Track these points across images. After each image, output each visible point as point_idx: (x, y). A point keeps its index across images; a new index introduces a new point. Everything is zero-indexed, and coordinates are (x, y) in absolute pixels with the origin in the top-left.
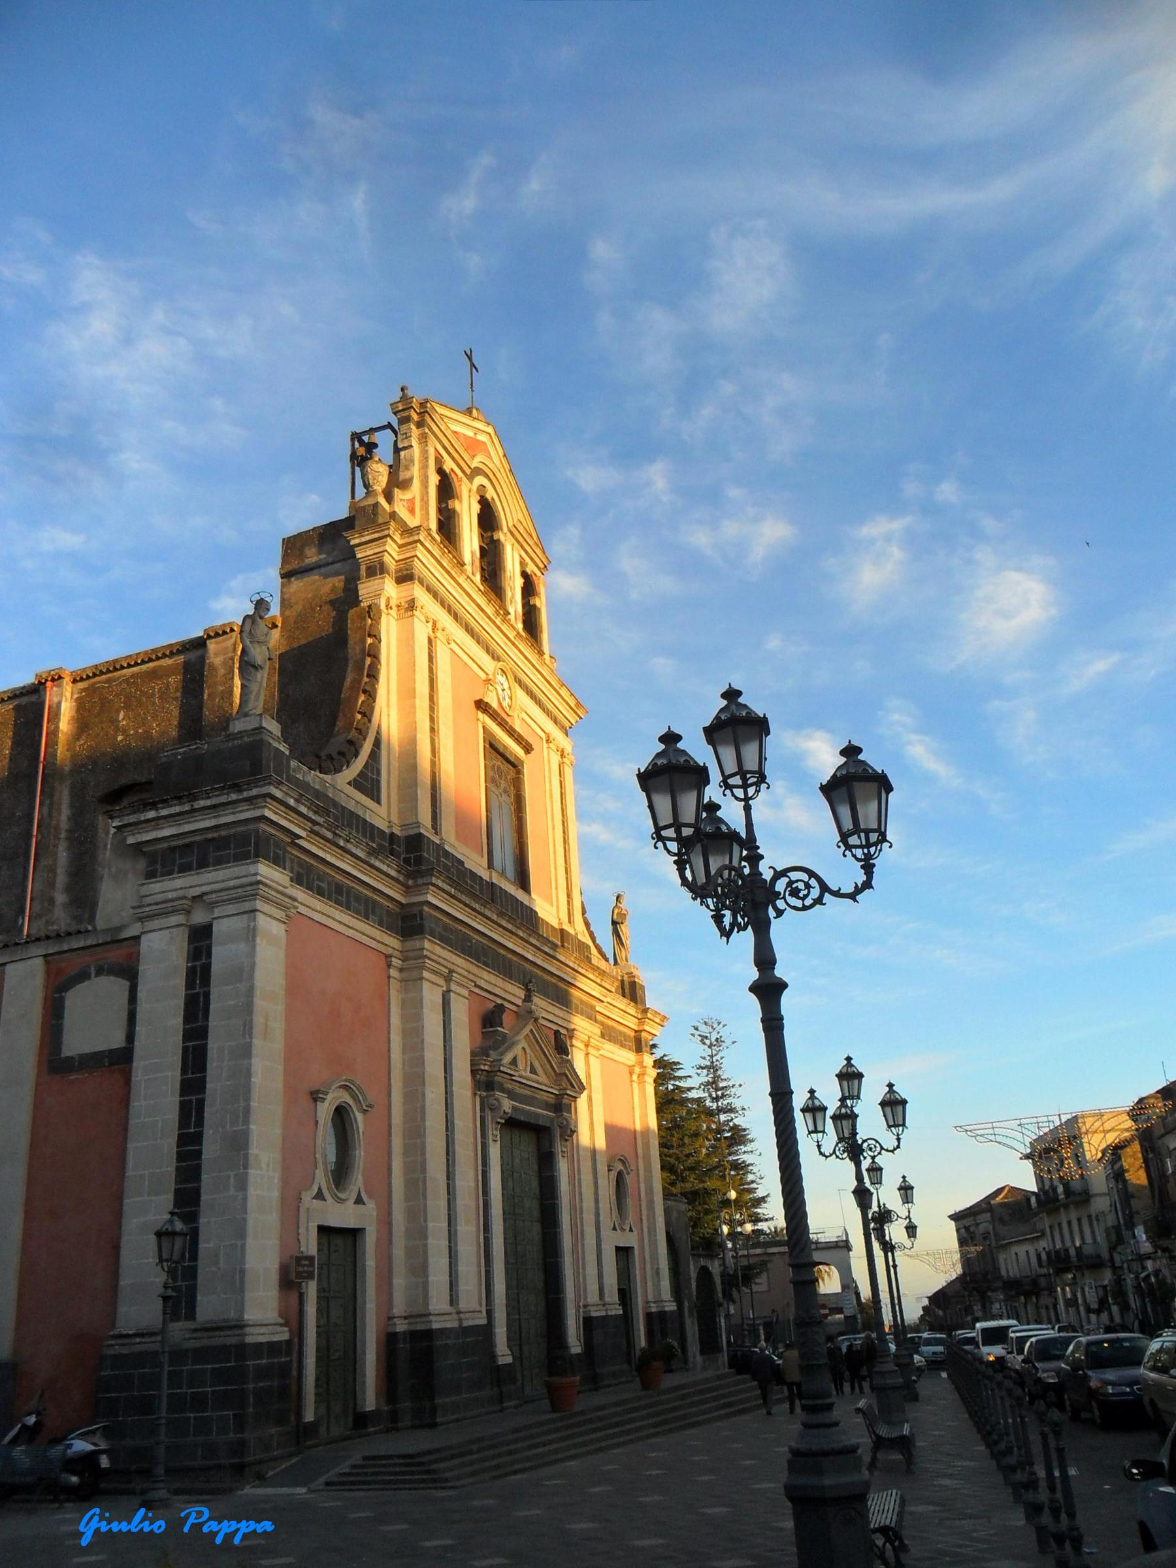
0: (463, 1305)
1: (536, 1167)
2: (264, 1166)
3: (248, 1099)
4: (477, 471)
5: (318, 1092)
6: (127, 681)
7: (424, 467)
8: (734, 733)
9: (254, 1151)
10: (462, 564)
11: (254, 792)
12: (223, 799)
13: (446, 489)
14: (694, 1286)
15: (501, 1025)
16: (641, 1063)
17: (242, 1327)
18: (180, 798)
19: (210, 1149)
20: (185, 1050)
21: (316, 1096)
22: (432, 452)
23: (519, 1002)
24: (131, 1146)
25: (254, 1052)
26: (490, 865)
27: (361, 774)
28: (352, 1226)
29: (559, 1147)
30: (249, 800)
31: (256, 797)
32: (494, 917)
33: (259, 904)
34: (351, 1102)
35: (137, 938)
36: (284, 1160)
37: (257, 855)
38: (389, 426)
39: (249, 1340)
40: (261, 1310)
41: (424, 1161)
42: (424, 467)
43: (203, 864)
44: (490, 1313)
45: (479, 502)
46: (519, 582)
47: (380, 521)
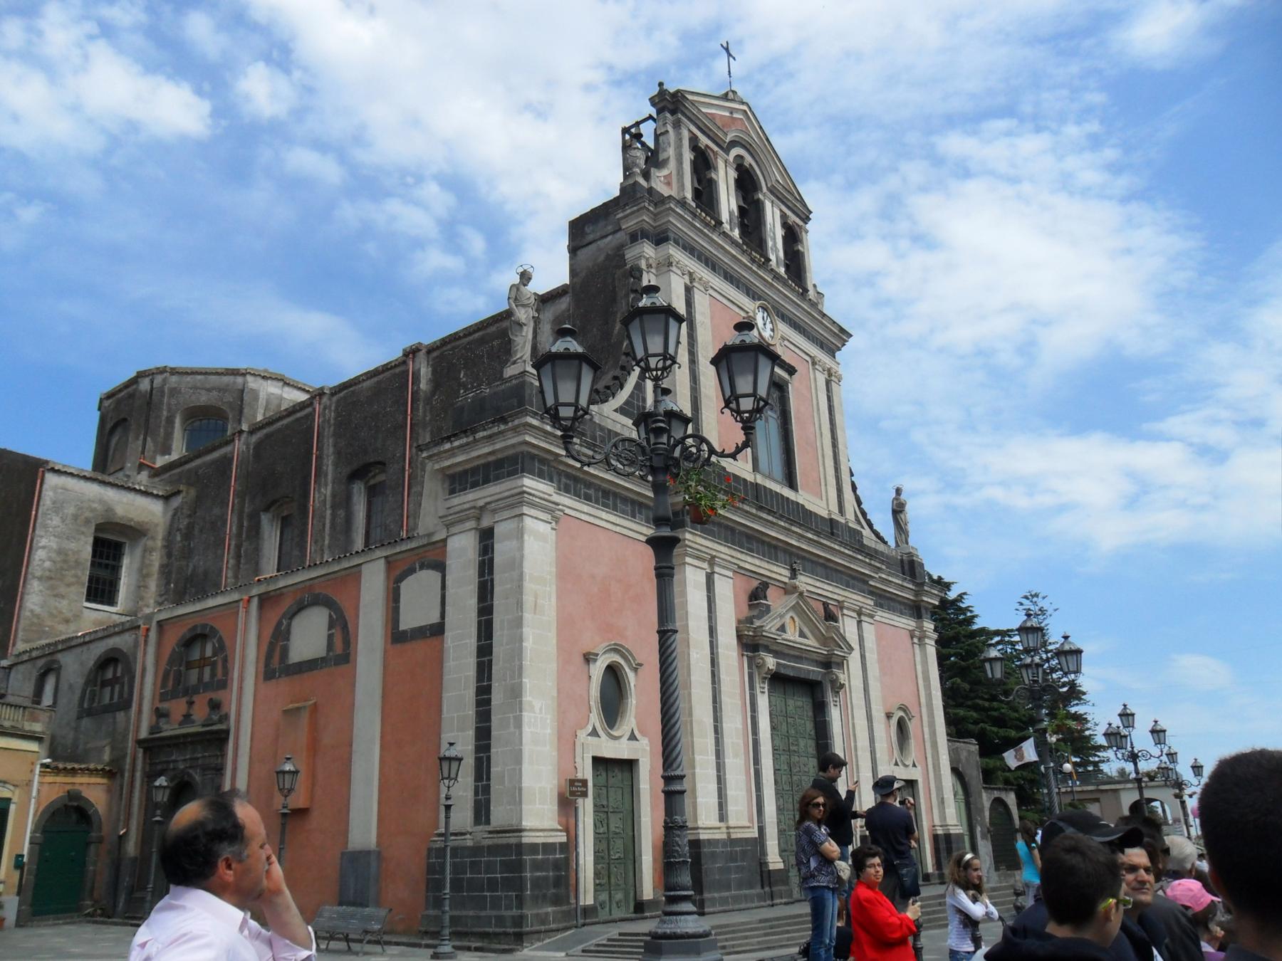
0: (732, 822)
1: (810, 714)
2: (537, 711)
3: (521, 659)
4: (734, 143)
5: (589, 653)
6: (465, 348)
7: (679, 147)
8: (642, 322)
9: (527, 698)
10: (720, 223)
11: (516, 422)
12: (495, 430)
13: (703, 164)
14: (987, 814)
15: (765, 598)
16: (920, 628)
17: (521, 831)
18: (465, 432)
19: (497, 697)
20: (479, 623)
21: (588, 658)
22: (686, 135)
23: (786, 580)
24: (446, 695)
25: (525, 622)
26: (756, 468)
27: (627, 403)
28: (626, 757)
29: (830, 698)
30: (514, 429)
31: (518, 426)
32: (754, 511)
33: (526, 510)
34: (622, 662)
35: (445, 541)
36: (559, 705)
37: (523, 471)
38: (650, 117)
39: (525, 840)
40: (538, 818)
41: (691, 708)
42: (679, 147)
43: (486, 481)
44: (761, 830)
45: (737, 169)
46: (779, 232)
47: (639, 195)
